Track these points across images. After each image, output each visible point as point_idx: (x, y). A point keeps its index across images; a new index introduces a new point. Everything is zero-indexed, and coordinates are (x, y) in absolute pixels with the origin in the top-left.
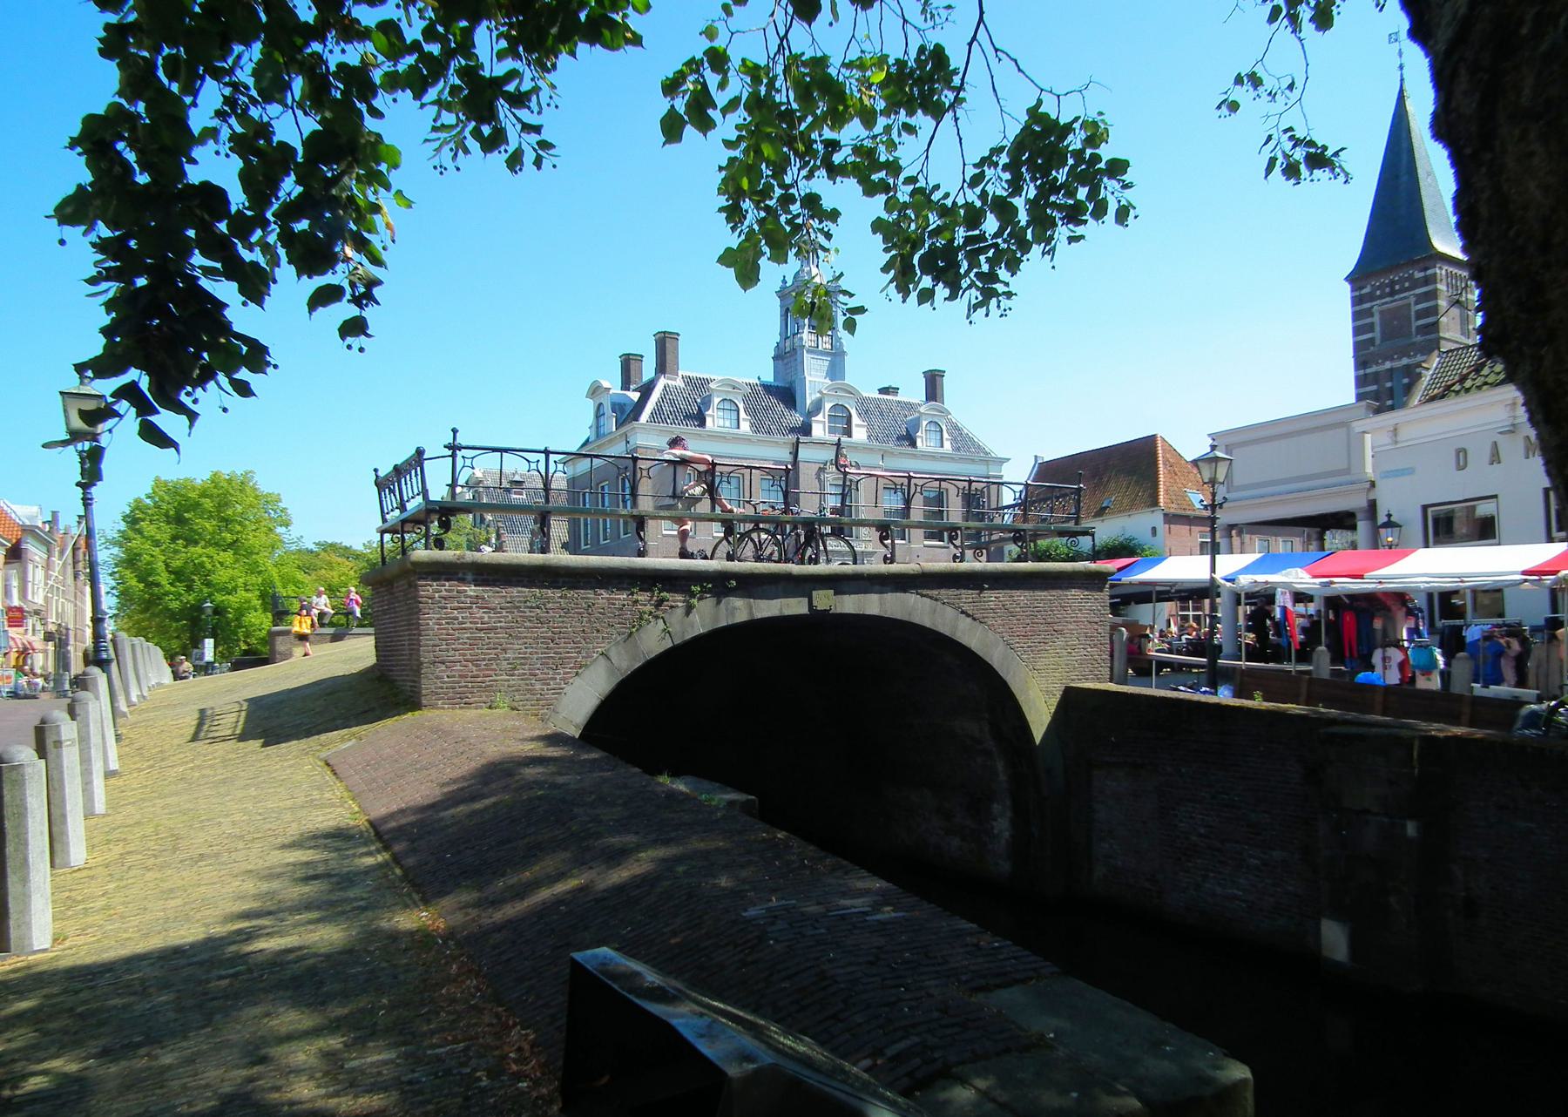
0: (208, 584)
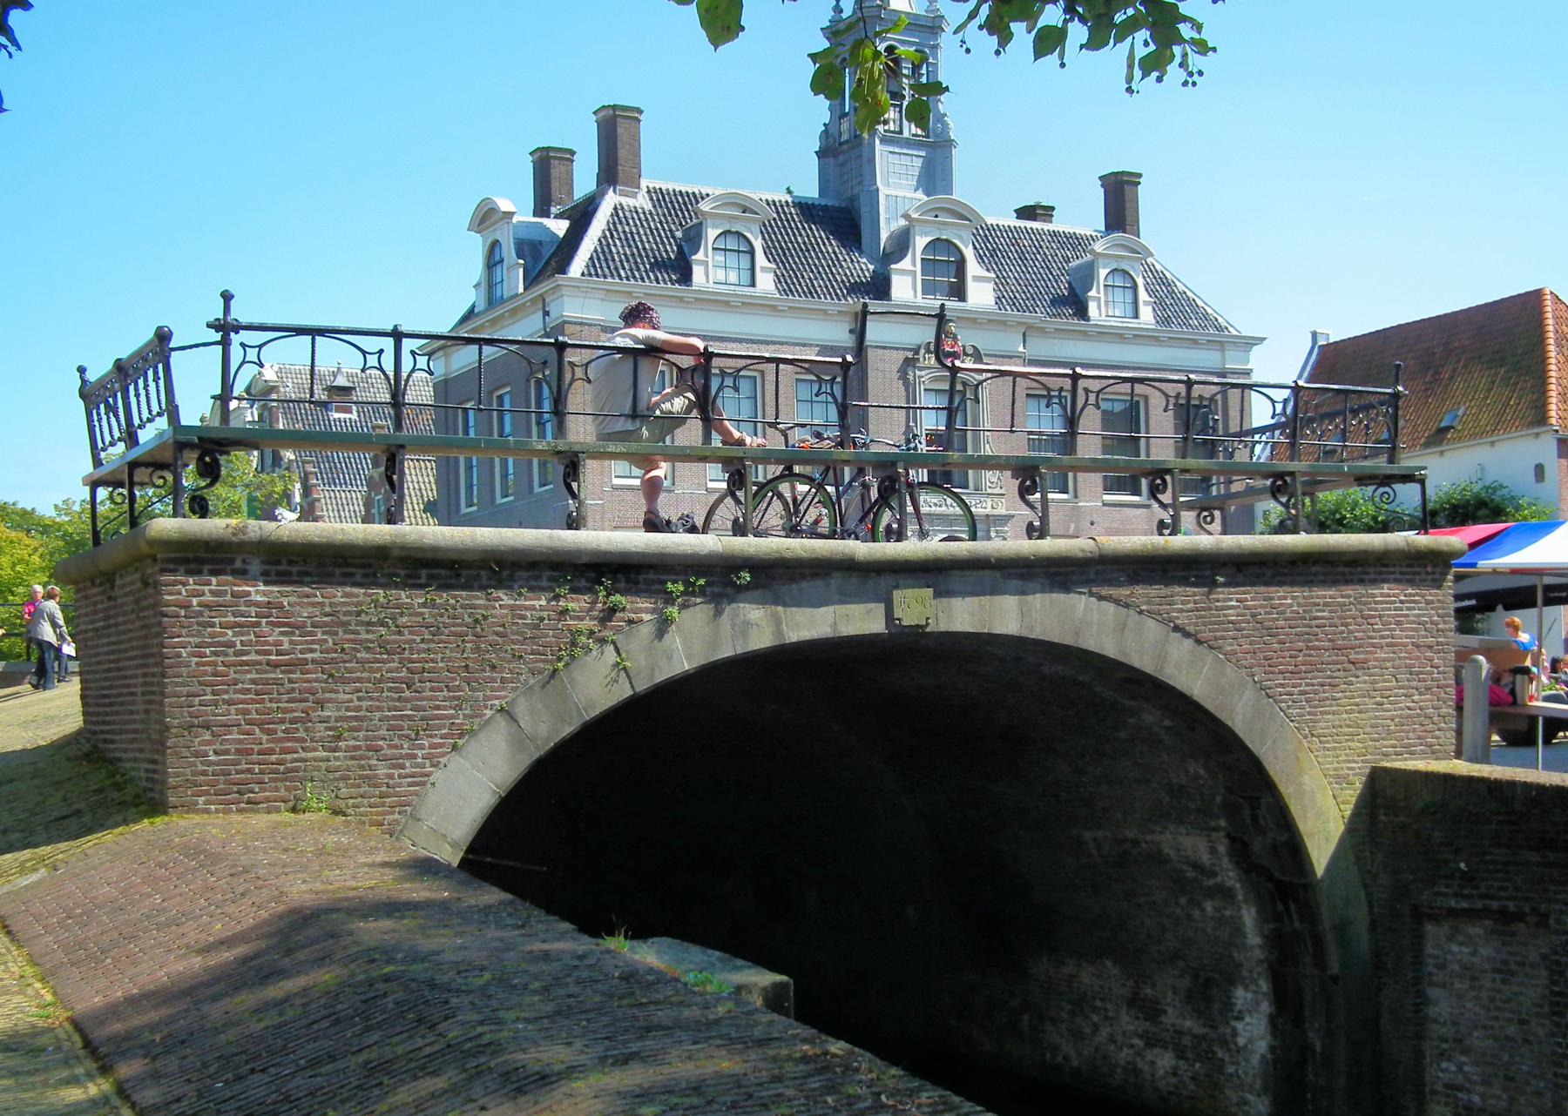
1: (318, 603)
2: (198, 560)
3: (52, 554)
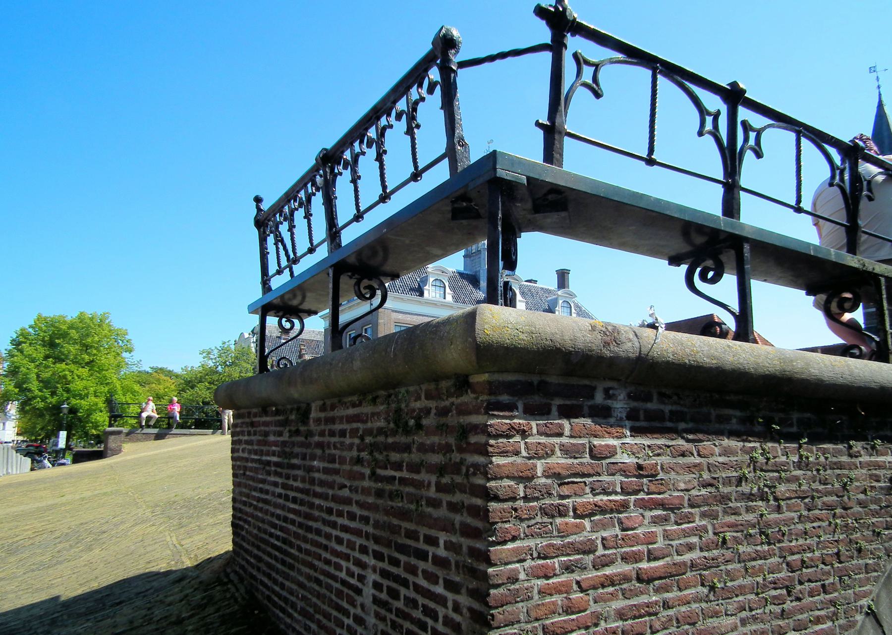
0: (68, 391)
1: (695, 466)
2: (542, 388)
3: (179, 385)
